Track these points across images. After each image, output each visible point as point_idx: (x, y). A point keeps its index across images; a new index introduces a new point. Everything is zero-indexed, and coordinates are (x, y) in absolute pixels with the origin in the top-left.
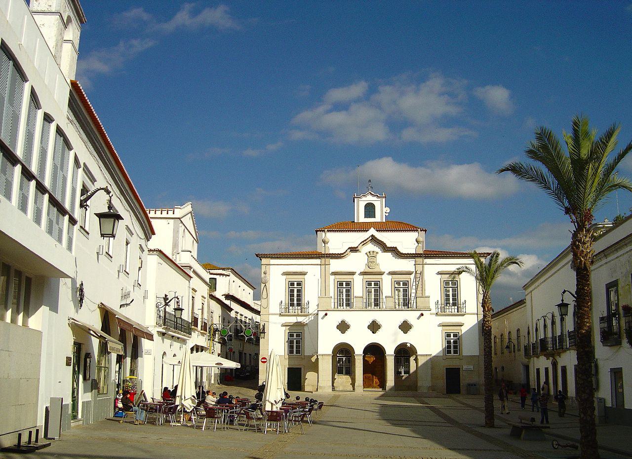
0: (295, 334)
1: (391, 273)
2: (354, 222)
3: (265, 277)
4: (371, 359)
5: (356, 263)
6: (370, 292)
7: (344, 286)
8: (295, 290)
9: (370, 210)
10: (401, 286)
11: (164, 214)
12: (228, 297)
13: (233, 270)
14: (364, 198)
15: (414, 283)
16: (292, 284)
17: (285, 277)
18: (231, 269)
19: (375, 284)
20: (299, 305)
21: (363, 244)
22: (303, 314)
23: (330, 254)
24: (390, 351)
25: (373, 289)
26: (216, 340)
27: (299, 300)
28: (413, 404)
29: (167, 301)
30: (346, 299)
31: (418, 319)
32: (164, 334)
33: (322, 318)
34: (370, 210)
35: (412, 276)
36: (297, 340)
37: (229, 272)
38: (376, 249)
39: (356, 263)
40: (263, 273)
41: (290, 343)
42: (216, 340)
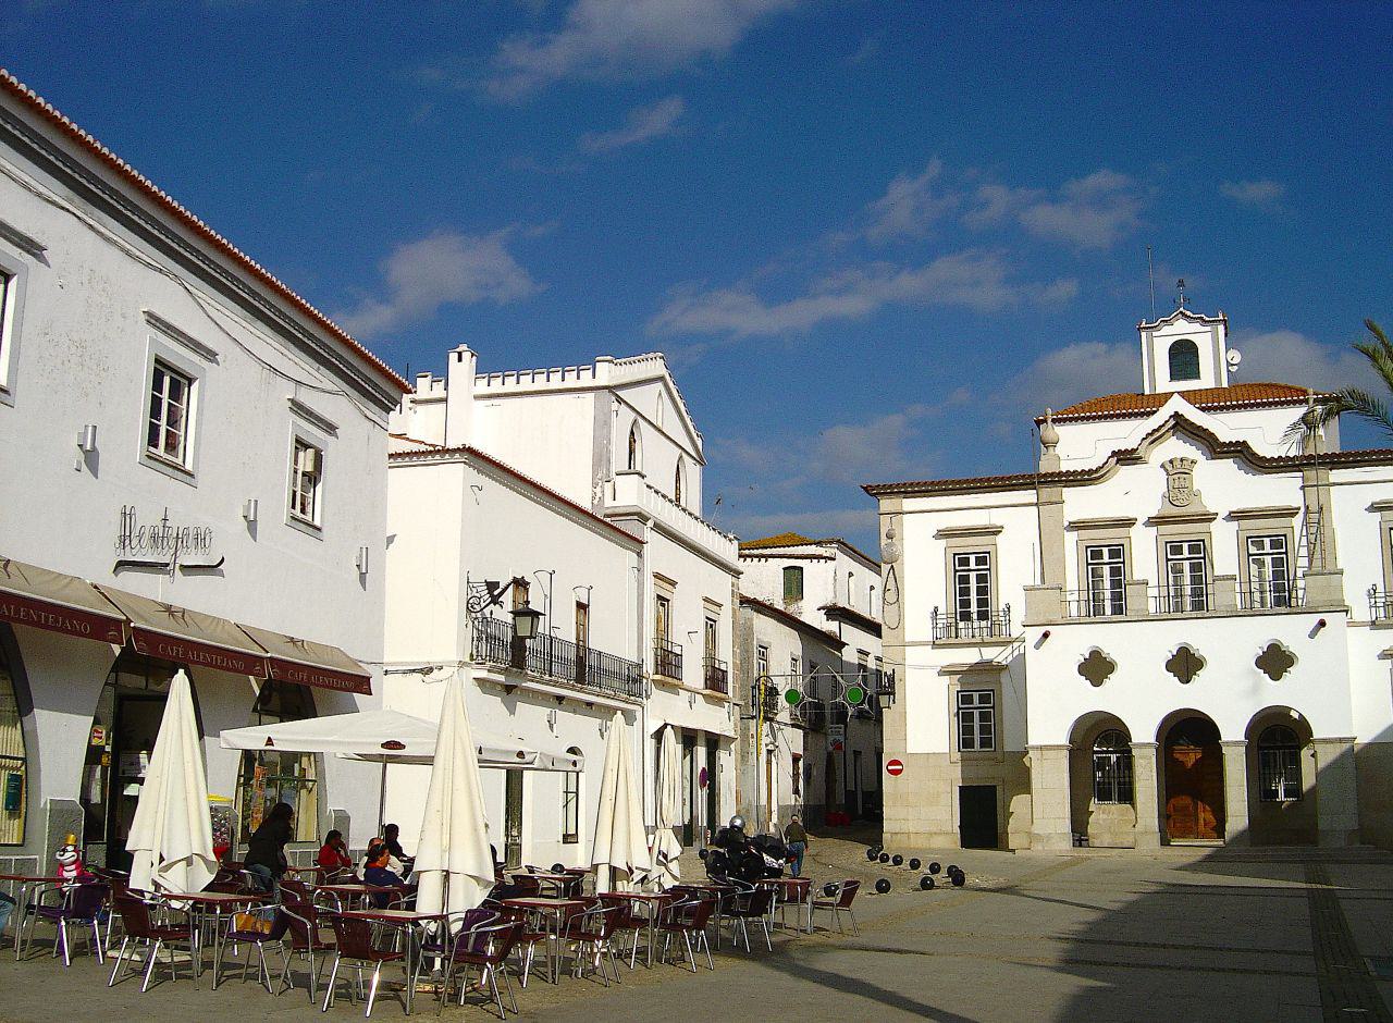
0: (976, 696)
1: (1235, 516)
2: (1143, 394)
3: (891, 545)
4: (1190, 756)
5: (1135, 494)
6: (1178, 571)
7: (1106, 559)
8: (973, 576)
9: (1184, 358)
10: (1267, 549)
11: (571, 381)
12: (833, 612)
13: (844, 544)
14: (1166, 330)
15: (1304, 539)
16: (964, 562)
17: (943, 543)
18: (838, 541)
19: (1192, 549)
20: (983, 616)
21: (1151, 439)
22: (994, 639)
23: (1060, 474)
24: (1233, 730)
25: (1186, 565)
26: (783, 716)
27: (983, 603)
28: (1284, 884)
29: (496, 593)
30: (1109, 588)
31: (1312, 635)
32: (509, 689)
33: (1038, 646)
34: (1184, 358)
35: (1297, 521)
36: (984, 706)
37: (834, 551)
38: (1189, 451)
39: (1135, 494)
40: (883, 536)
41: (965, 718)
42: (783, 716)
